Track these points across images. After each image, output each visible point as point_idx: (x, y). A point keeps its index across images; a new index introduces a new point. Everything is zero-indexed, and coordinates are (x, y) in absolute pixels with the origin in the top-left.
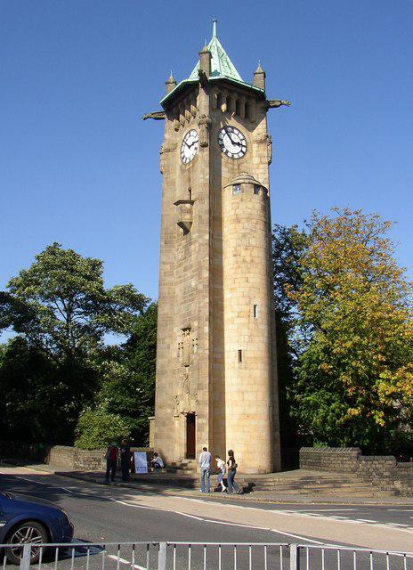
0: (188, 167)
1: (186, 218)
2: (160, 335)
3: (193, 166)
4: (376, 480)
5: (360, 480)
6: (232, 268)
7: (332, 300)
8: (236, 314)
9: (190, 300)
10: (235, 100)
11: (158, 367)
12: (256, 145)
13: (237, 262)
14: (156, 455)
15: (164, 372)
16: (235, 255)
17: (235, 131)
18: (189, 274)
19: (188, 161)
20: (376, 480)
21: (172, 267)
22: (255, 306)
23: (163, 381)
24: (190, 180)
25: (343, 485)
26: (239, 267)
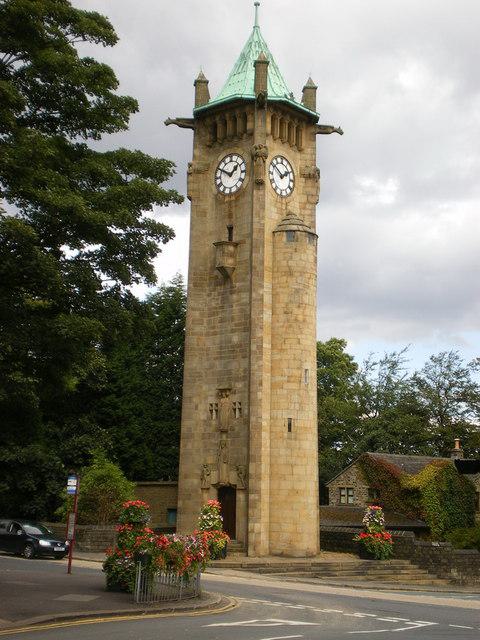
0: (227, 199)
1: (229, 262)
2: (187, 392)
3: (237, 199)
4: (432, 567)
5: (415, 566)
6: (283, 326)
7: (388, 418)
8: (286, 378)
9: (229, 357)
10: (287, 122)
11: (184, 430)
12: (303, 180)
13: (288, 321)
14: (117, 585)
15: (191, 436)
16: (285, 313)
17: (285, 162)
18: (230, 326)
19: (227, 191)
20: (432, 567)
21: (202, 315)
22: (306, 370)
23: (189, 446)
24: (230, 216)
25: (403, 571)
26: (290, 326)
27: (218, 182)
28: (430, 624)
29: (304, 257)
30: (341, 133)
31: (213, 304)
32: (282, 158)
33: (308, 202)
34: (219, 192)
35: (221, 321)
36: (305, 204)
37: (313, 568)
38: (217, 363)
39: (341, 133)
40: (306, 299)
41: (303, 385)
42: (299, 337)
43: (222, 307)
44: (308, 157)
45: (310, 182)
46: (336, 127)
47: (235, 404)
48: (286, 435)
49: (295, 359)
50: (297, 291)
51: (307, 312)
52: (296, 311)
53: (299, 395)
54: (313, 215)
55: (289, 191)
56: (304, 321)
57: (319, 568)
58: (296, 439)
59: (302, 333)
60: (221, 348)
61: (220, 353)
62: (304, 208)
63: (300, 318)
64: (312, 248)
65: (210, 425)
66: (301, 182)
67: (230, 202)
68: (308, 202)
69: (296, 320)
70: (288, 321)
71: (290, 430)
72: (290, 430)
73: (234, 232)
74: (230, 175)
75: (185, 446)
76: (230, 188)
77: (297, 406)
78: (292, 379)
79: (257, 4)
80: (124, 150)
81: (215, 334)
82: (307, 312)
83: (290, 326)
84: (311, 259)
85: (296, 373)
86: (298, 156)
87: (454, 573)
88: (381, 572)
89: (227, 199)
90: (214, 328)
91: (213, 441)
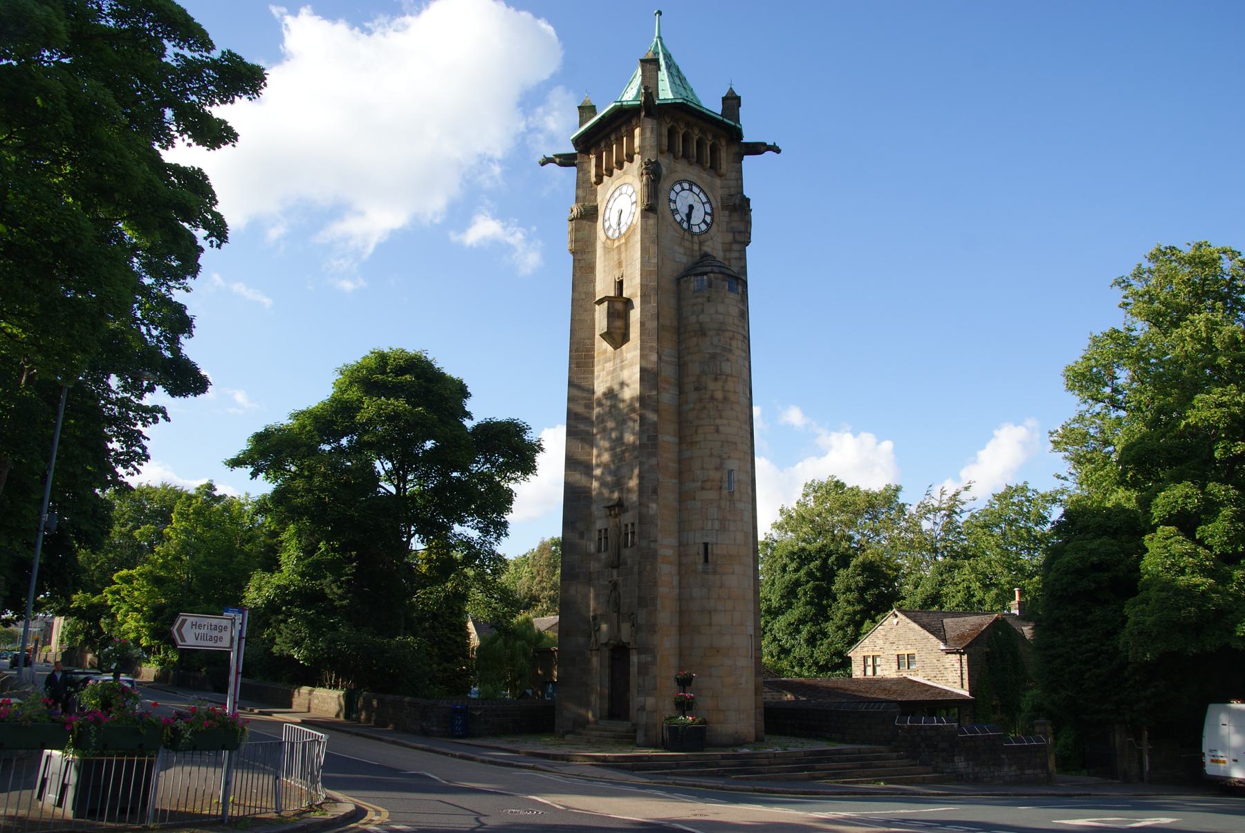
0: (616, 244)
12: (727, 213)
17: (695, 189)
24: (620, 264)
26: (704, 408)
29: (721, 309)
30: (778, 151)
32: (691, 183)
33: (735, 241)
36: (731, 243)
37: (723, 762)
39: (778, 151)
40: (727, 368)
41: (725, 492)
42: (718, 422)
44: (733, 183)
45: (736, 216)
46: (770, 143)
48: (700, 567)
49: (711, 455)
50: (713, 357)
51: (730, 386)
52: (711, 385)
53: (719, 507)
54: (743, 258)
55: (703, 227)
56: (725, 399)
57: (732, 762)
58: (715, 573)
59: (721, 417)
62: (730, 250)
63: (719, 395)
64: (732, 297)
66: (723, 216)
67: (619, 247)
68: (735, 241)
69: (712, 398)
70: (700, 400)
71: (706, 560)
72: (706, 560)
73: (625, 286)
77: (717, 525)
78: (708, 485)
80: (208, 34)
82: (730, 386)
83: (704, 408)
84: (734, 311)
85: (715, 475)
86: (718, 182)
87: (961, 764)
88: (840, 765)
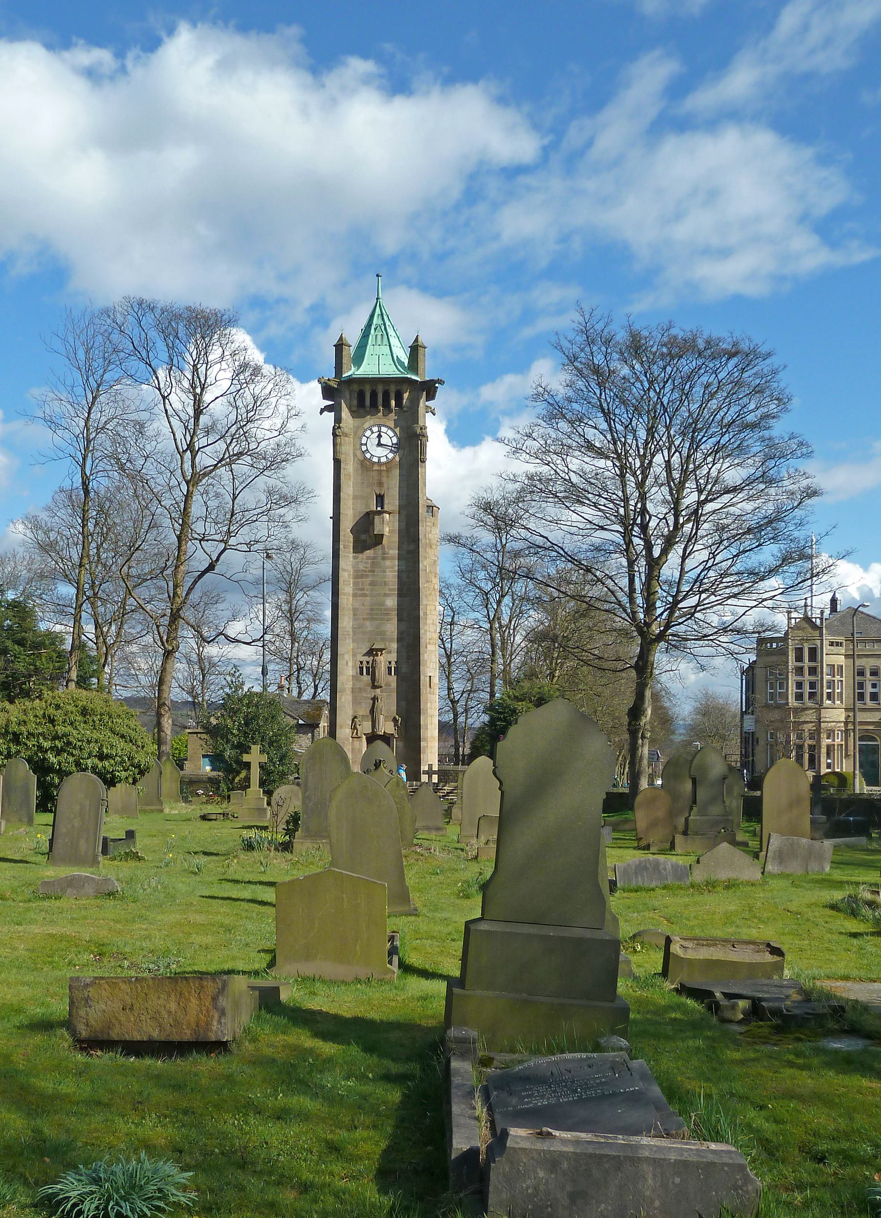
0: (376, 467)
23: (343, 700)
27: (364, 448)
28: (405, 401)
31: (361, 567)
34: (365, 458)
35: (372, 584)
38: (368, 623)
43: (373, 571)
47: (390, 663)
60: (371, 610)
61: (371, 614)
65: (361, 681)
67: (380, 471)
74: (379, 444)
75: (340, 699)
76: (379, 458)
79: (378, 276)
81: (364, 595)
89: (376, 467)
90: (363, 589)
91: (390, 1121)
